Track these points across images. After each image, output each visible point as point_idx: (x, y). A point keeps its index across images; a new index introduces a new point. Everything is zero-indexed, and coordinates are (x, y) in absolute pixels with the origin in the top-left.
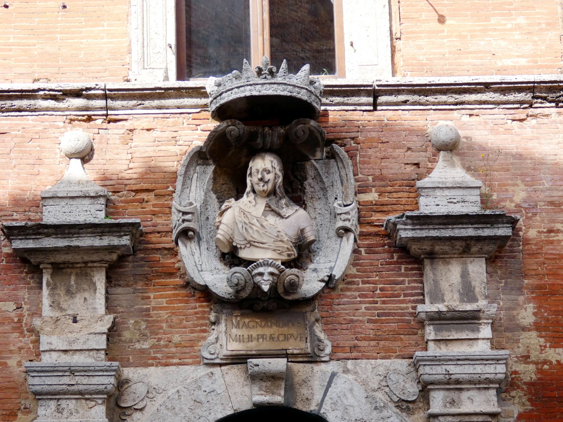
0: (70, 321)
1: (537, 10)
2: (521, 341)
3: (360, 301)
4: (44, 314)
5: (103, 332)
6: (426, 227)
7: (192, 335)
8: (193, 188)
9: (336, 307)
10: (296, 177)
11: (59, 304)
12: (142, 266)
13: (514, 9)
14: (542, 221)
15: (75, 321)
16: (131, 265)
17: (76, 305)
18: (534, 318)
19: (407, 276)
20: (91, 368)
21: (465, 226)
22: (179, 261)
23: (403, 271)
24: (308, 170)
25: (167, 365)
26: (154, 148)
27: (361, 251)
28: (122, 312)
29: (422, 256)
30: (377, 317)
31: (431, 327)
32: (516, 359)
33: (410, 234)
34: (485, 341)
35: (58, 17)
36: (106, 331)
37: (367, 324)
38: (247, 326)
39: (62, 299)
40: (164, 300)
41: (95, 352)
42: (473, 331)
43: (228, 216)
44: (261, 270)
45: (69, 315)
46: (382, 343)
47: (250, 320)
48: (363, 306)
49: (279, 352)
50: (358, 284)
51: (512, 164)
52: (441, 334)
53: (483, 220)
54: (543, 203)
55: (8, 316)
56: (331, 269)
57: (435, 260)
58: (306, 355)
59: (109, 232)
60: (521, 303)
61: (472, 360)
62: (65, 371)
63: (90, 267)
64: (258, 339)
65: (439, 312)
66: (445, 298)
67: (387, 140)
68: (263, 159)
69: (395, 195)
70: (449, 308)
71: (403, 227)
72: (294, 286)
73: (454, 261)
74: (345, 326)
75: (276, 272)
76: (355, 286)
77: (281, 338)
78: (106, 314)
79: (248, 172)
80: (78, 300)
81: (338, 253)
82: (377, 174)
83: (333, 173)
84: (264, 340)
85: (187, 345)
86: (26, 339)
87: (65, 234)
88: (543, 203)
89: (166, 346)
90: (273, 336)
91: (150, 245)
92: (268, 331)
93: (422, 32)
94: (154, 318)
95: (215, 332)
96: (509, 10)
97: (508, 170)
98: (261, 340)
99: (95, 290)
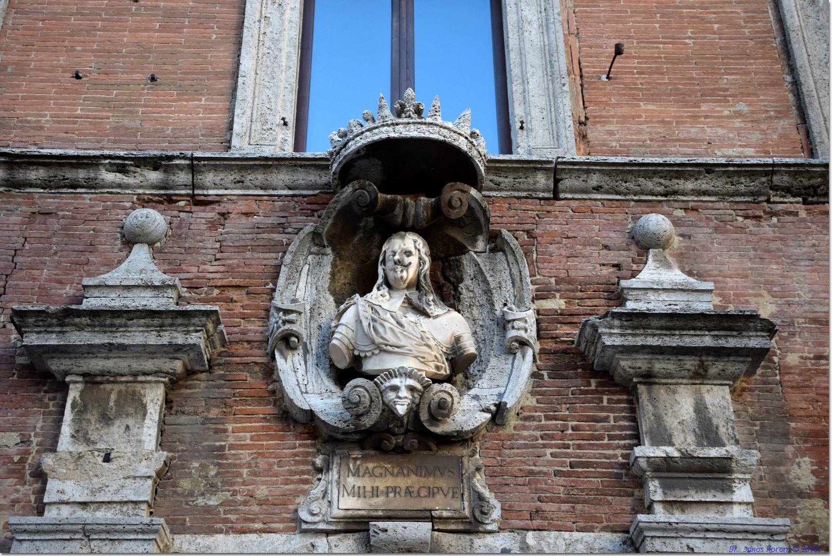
0: (100, 460)
1: (762, 97)
2: (799, 512)
3: (544, 445)
4: (60, 448)
5: (148, 475)
6: (642, 331)
7: (287, 487)
8: (302, 284)
9: (507, 451)
10: (446, 278)
11: (87, 433)
12: (219, 387)
13: (730, 96)
14: (805, 343)
15: (107, 459)
16: (203, 385)
17: (113, 436)
18: (814, 478)
19: (612, 410)
20: (118, 527)
21: (698, 332)
22: (275, 381)
23: (605, 403)
24: (465, 267)
25: (244, 532)
26: (254, 236)
27: (543, 375)
28: (183, 451)
29: (635, 380)
30: (569, 469)
31: (656, 483)
32: (795, 541)
33: (618, 341)
34: (744, 507)
35: (143, 89)
36: (154, 474)
37: (554, 478)
38: (372, 475)
39: (93, 427)
40: (248, 435)
41: (131, 506)
42: (723, 491)
43: (348, 317)
44: (396, 381)
45: (99, 450)
46: (579, 507)
47: (376, 465)
48: (549, 451)
49: (420, 514)
50: (540, 421)
51: (750, 269)
52: (674, 493)
53: (726, 325)
54: (803, 320)
55: (5, 453)
56: (500, 395)
57: (654, 386)
58: (461, 519)
59: (171, 325)
60: (790, 456)
61: (729, 532)
62: (75, 532)
63: (142, 382)
64: (387, 494)
65: (668, 459)
66: (674, 440)
67: (574, 235)
68: (403, 238)
69: (589, 302)
70: (682, 453)
71: (607, 330)
72: (442, 410)
73: (681, 389)
74: (520, 480)
75: (419, 386)
76: (536, 423)
77: (424, 492)
78: (157, 450)
79: (381, 259)
80: (117, 429)
81: (510, 375)
82: (562, 275)
83: (501, 271)
84: (397, 495)
85: (275, 502)
86: (27, 487)
87: (105, 326)
88: (803, 320)
89: (245, 503)
90: (411, 489)
91: (234, 359)
92: (402, 482)
93: (613, 117)
94: (230, 461)
95: (322, 482)
96: (725, 96)
97: (746, 277)
98: (391, 495)
99: (145, 415)
